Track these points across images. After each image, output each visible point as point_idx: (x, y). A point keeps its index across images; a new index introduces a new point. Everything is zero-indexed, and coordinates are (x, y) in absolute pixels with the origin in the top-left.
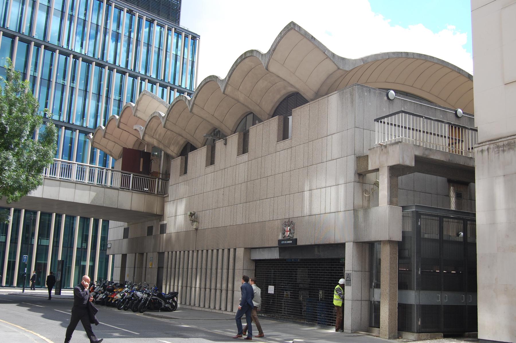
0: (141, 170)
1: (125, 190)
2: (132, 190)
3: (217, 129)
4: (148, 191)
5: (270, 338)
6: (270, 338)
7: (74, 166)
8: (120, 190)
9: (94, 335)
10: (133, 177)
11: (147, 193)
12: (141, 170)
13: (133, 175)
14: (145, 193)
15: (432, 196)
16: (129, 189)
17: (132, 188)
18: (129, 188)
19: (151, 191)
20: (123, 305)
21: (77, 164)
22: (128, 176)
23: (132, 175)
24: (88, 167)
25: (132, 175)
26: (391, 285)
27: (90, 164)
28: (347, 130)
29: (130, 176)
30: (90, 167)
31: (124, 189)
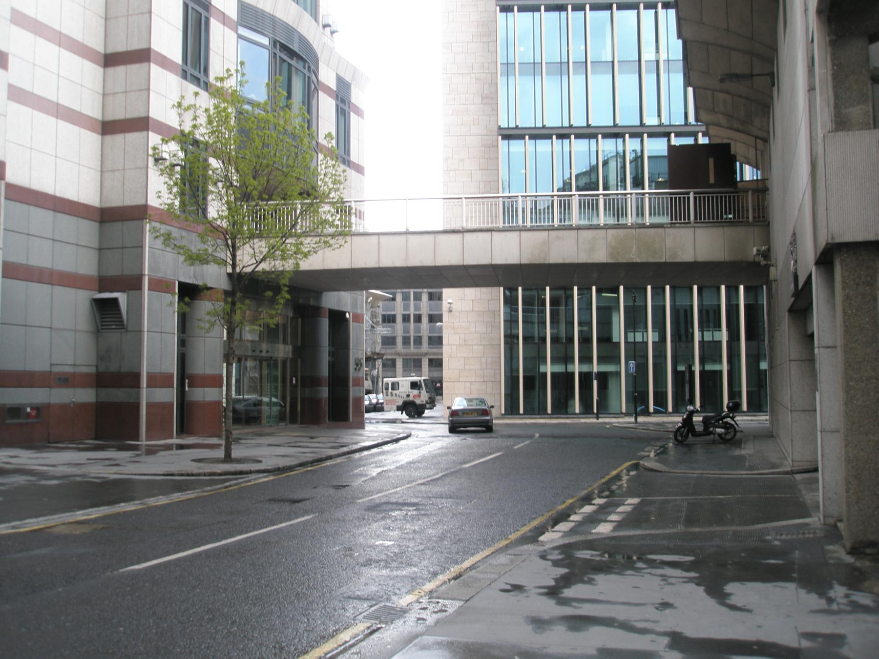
0: (712, 181)
1: (677, 225)
2: (696, 223)
3: (289, 109)
4: (733, 220)
5: (685, 580)
6: (685, 580)
7: (573, 200)
8: (667, 227)
9: (525, 586)
10: (695, 198)
11: (726, 224)
12: (712, 181)
13: (695, 193)
14: (724, 224)
15: (129, 169)
16: (690, 223)
17: (696, 218)
18: (689, 219)
19: (739, 218)
20: (607, 497)
21: (520, 197)
22: (684, 198)
23: (691, 196)
24: (601, 196)
25: (691, 196)
26: (851, 384)
27: (649, 189)
28: (59, 75)
29: (689, 198)
30: (604, 195)
31: (675, 223)
